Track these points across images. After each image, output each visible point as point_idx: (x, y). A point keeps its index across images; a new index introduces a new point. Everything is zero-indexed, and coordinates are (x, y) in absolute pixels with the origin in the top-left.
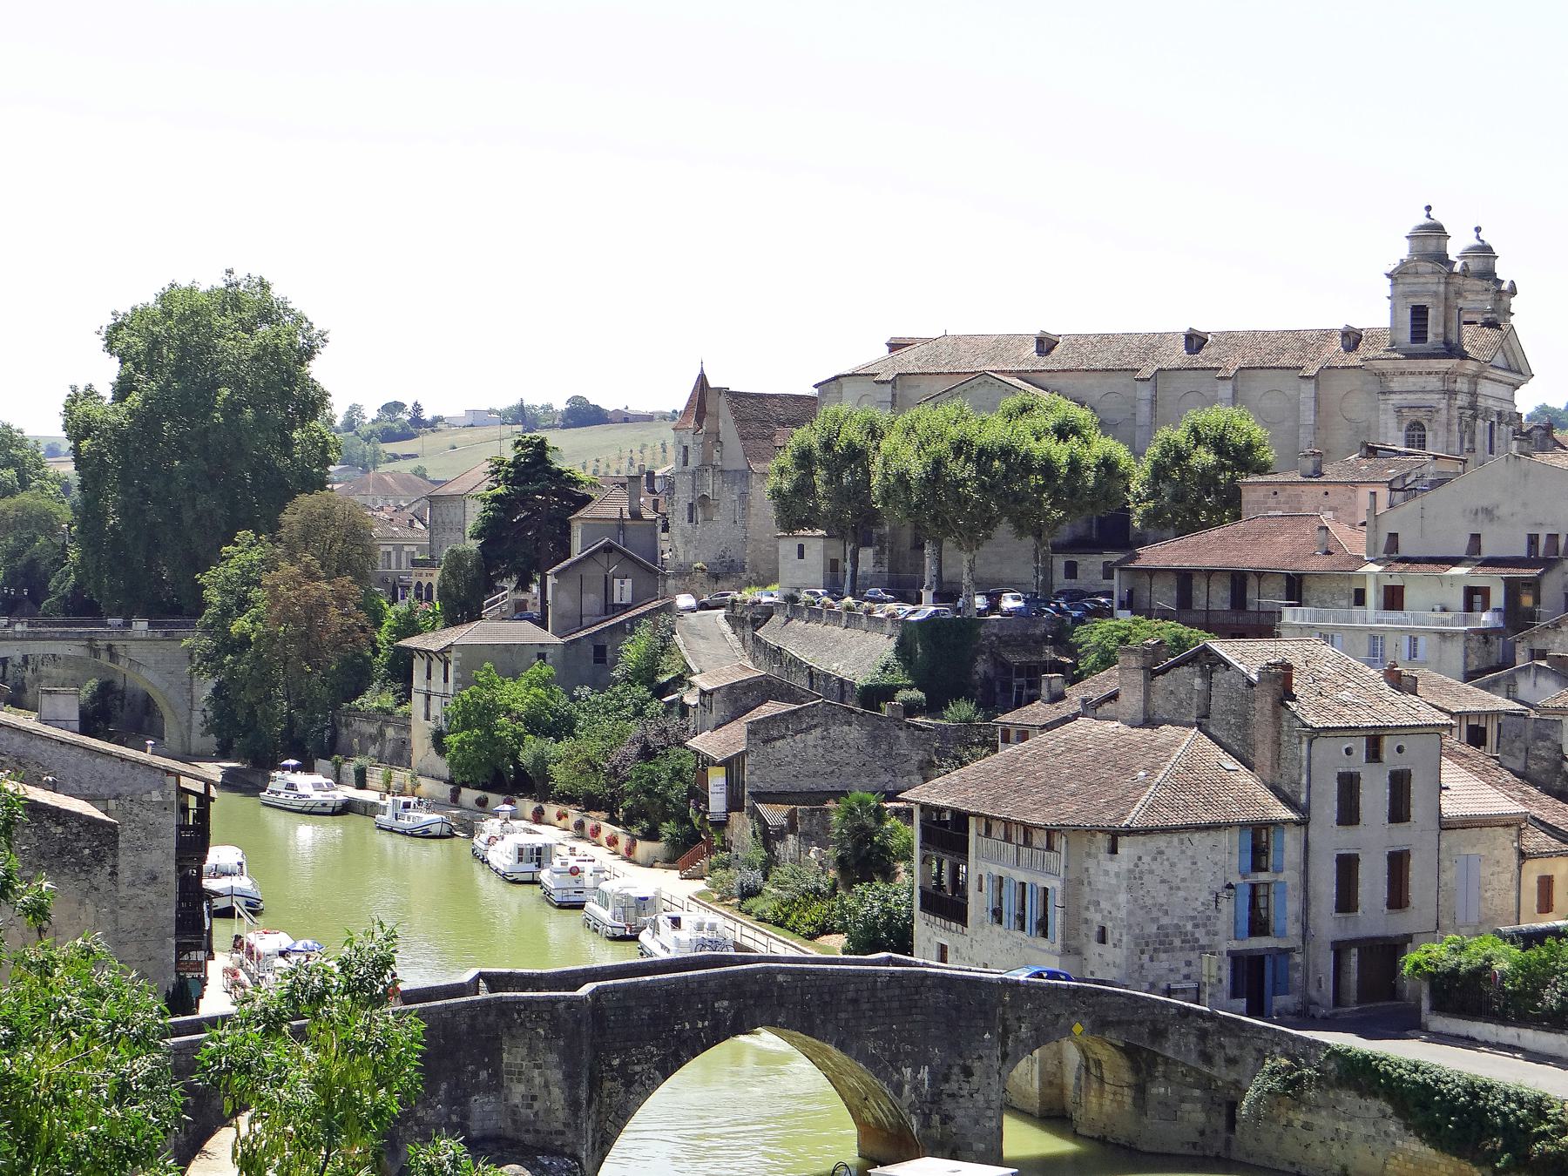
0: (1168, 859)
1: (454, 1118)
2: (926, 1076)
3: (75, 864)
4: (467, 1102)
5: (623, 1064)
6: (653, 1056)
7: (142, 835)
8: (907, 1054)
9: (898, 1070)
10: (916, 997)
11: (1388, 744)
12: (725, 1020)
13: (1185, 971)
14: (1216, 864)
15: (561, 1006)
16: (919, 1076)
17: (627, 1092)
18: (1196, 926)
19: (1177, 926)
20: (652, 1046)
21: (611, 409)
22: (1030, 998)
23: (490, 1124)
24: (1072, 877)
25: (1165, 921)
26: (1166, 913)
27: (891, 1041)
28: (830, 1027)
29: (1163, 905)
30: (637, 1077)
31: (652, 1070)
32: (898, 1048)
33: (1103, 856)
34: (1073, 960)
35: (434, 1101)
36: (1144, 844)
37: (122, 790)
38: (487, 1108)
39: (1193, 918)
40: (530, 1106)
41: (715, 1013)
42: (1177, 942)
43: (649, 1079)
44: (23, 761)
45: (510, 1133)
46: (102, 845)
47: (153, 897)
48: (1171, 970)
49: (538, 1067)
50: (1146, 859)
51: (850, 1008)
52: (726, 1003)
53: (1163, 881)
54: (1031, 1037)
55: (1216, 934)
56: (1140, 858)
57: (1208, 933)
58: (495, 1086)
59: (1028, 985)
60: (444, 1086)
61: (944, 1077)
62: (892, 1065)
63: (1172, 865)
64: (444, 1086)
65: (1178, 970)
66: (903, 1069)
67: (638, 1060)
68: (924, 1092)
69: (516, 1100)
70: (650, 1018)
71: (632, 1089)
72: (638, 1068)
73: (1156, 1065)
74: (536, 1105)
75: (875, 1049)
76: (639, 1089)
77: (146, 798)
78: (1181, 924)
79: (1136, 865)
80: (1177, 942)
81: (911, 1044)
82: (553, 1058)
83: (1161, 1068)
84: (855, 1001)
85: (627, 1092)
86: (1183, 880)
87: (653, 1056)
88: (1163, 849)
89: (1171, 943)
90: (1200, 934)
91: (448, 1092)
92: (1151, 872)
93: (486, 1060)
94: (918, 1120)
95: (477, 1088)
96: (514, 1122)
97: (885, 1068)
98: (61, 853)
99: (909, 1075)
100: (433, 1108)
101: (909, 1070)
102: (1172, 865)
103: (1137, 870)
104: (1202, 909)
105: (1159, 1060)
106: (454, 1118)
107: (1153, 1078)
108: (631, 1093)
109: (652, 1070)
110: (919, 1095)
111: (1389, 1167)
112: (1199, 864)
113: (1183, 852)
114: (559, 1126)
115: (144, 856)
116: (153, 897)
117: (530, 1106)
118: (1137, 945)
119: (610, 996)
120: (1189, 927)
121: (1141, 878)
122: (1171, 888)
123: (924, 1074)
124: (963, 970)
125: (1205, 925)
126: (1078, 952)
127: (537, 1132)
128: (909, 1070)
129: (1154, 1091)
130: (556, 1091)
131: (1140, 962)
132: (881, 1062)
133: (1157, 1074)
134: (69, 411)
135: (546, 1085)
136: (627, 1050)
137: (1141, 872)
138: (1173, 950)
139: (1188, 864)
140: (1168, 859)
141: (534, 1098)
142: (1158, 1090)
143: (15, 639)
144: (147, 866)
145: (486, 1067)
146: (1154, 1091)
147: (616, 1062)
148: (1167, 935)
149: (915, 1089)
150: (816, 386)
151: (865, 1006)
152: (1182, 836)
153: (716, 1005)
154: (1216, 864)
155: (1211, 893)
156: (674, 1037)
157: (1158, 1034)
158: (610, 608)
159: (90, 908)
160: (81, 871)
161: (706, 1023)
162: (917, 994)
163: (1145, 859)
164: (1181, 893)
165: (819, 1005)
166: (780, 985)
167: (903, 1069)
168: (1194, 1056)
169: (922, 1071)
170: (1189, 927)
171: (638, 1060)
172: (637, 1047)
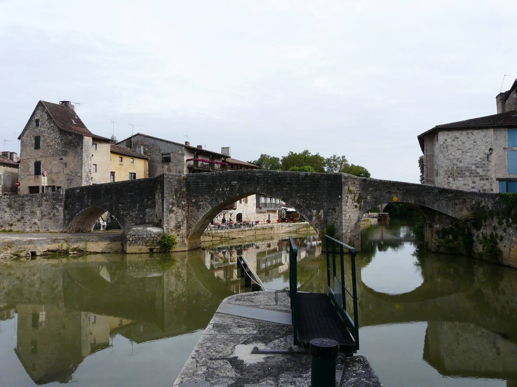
0: (461, 140)
1: (141, 216)
2: (322, 214)
3: (73, 146)
4: (145, 211)
5: (197, 202)
6: (207, 199)
7: (177, 162)
8: (314, 205)
9: (310, 211)
10: (318, 183)
12: (236, 188)
13: (473, 185)
14: (487, 142)
16: (320, 214)
17: (198, 211)
18: (478, 167)
19: (466, 167)
20: (207, 196)
22: (372, 186)
25: (460, 165)
26: (461, 162)
28: (279, 193)
29: (459, 159)
30: (201, 206)
31: (207, 204)
36: (448, 135)
37: (174, 151)
39: (475, 164)
41: (232, 186)
42: (467, 173)
43: (206, 207)
44: (154, 145)
46: (79, 141)
48: (465, 185)
52: (236, 182)
54: (373, 201)
55: (488, 171)
56: (446, 140)
57: (484, 170)
62: (307, 208)
64: (138, 205)
65: (468, 185)
66: (312, 210)
67: (202, 200)
68: (322, 219)
70: (206, 186)
71: (200, 210)
72: (202, 203)
75: (299, 202)
77: (178, 152)
78: (469, 166)
79: (444, 143)
80: (467, 173)
81: (317, 201)
83: (437, 217)
85: (198, 211)
86: (469, 149)
87: (207, 199)
88: (458, 136)
89: (464, 174)
90: (479, 170)
91: (139, 207)
92: (452, 146)
93: (150, 198)
94: (319, 230)
97: (304, 209)
98: (70, 143)
99: (315, 213)
100: (134, 212)
101: (315, 211)
103: (445, 145)
104: (480, 160)
105: (437, 213)
106: (141, 216)
108: (199, 212)
109: (207, 204)
110: (320, 221)
111: (512, 252)
112: (478, 142)
113: (469, 138)
118: (446, 174)
119: (191, 178)
120: (474, 167)
121: (447, 148)
122: (463, 152)
123: (322, 212)
125: (482, 167)
128: (315, 211)
129: (435, 226)
131: (448, 181)
132: (302, 207)
133: (436, 219)
136: (198, 197)
137: (447, 146)
138: (466, 177)
139: (472, 142)
140: (461, 140)
144: (178, 170)
145: (150, 200)
146: (435, 226)
147: (194, 201)
148: (462, 171)
151: (294, 186)
152: (468, 131)
153: (232, 183)
154: (487, 142)
155: (485, 154)
156: (215, 193)
159: (77, 158)
160: (75, 148)
161: (228, 189)
162: (318, 182)
163: (448, 140)
164: (469, 154)
165: (274, 185)
166: (258, 177)
167: (312, 210)
169: (321, 212)
170: (474, 167)
171: (202, 200)
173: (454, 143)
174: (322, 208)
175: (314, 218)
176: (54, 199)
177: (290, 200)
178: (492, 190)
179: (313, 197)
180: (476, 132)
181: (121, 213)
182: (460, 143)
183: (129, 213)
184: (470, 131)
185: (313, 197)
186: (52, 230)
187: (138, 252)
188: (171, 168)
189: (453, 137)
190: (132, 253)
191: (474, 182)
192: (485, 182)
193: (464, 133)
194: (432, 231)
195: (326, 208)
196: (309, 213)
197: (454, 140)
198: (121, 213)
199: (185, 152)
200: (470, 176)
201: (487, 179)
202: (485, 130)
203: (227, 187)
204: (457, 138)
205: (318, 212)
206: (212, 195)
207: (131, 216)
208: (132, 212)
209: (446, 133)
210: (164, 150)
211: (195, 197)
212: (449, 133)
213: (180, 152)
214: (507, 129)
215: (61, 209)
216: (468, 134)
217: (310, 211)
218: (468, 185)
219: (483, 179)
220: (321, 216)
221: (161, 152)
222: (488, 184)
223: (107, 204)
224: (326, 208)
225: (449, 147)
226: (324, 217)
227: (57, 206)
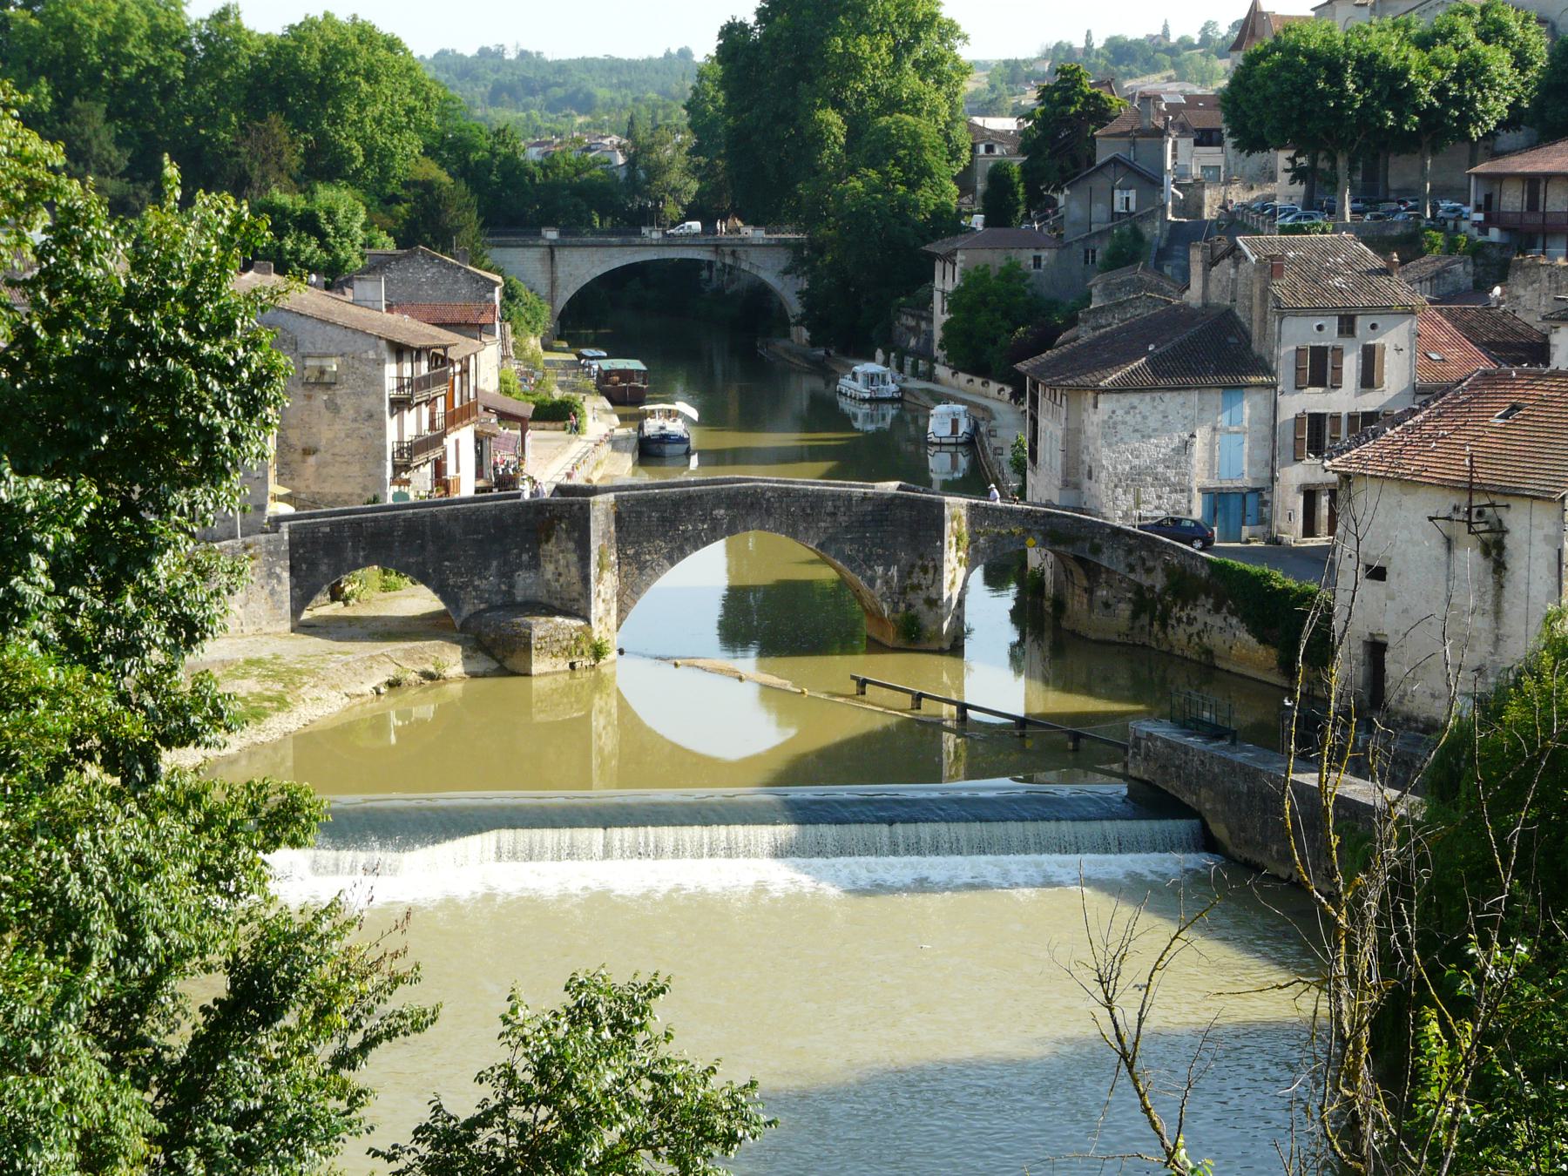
1: (503, 587)
5: (637, 554)
8: (879, 557)
9: (871, 568)
11: (1362, 323)
13: (1156, 502)
15: (577, 507)
21: (1141, 36)
23: (531, 592)
24: (1072, 426)
25: (1136, 462)
27: (865, 545)
32: (870, 550)
33: (1091, 410)
34: (1072, 494)
35: (487, 574)
36: (1118, 401)
37: (347, 349)
38: (529, 581)
40: (557, 581)
41: (714, 519)
45: (545, 600)
47: (370, 430)
49: (563, 552)
50: (1120, 412)
51: (829, 519)
53: (1136, 431)
56: (1114, 412)
58: (535, 564)
59: (895, 497)
60: (495, 563)
61: (906, 574)
63: (1145, 418)
64: (495, 563)
69: (549, 576)
72: (648, 557)
73: (1100, 573)
74: (562, 580)
76: (650, 572)
79: (1110, 417)
80: (1149, 479)
82: (571, 545)
83: (1104, 576)
84: (834, 514)
86: (1155, 430)
90: (1171, 474)
92: (1124, 423)
95: (520, 567)
96: (548, 591)
97: (860, 566)
102: (1145, 418)
107: (1099, 584)
113: (1155, 407)
114: (575, 595)
115: (364, 399)
116: (370, 430)
117: (557, 581)
120: (1160, 469)
122: (1143, 437)
123: (894, 571)
124: (769, 481)
126: (1077, 487)
127: (562, 599)
130: (573, 570)
134: (1204, 29)
135: (567, 566)
136: (640, 544)
139: (1160, 416)
141: (560, 575)
142: (1102, 593)
143: (652, 245)
144: (367, 406)
145: (528, 551)
149: (887, 582)
150: (1313, 9)
157: (1097, 550)
158: (1116, 217)
163: (1118, 413)
168: (1123, 566)
172: (648, 541)
173: (1128, 418)
174: (896, 562)
175: (879, 581)
176: (270, 553)
177: (833, 547)
178: (1190, 512)
179: (878, 541)
180: (1168, 396)
181: (451, 582)
182: (1139, 418)
183: (471, 581)
184: (1157, 395)
185: (878, 541)
186: (268, 630)
187: (551, 670)
188: (339, 401)
189: (1128, 406)
190: (540, 675)
191: (1159, 497)
192: (1179, 496)
193: (1148, 397)
194: (1090, 601)
195: (903, 562)
196: (869, 573)
197: (1127, 413)
198: (451, 582)
199: (386, 355)
200: (1152, 485)
201: (1182, 491)
202: (1183, 393)
203: (703, 522)
204: (1134, 408)
205: (887, 570)
206: (673, 539)
207: (476, 588)
208: (480, 578)
209: (1115, 396)
210: (313, 344)
211: (633, 543)
212: (1120, 396)
213: (371, 355)
214: (1221, 390)
215: (286, 575)
216: (1153, 399)
217: (871, 568)
218: (1150, 503)
219: (1176, 491)
220: (893, 576)
221: (302, 351)
222: (1185, 501)
223: (411, 560)
224: (903, 562)
225: (1120, 427)
226: (899, 581)
227: (278, 570)
